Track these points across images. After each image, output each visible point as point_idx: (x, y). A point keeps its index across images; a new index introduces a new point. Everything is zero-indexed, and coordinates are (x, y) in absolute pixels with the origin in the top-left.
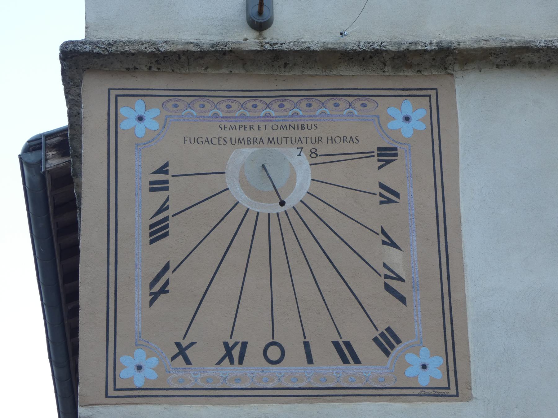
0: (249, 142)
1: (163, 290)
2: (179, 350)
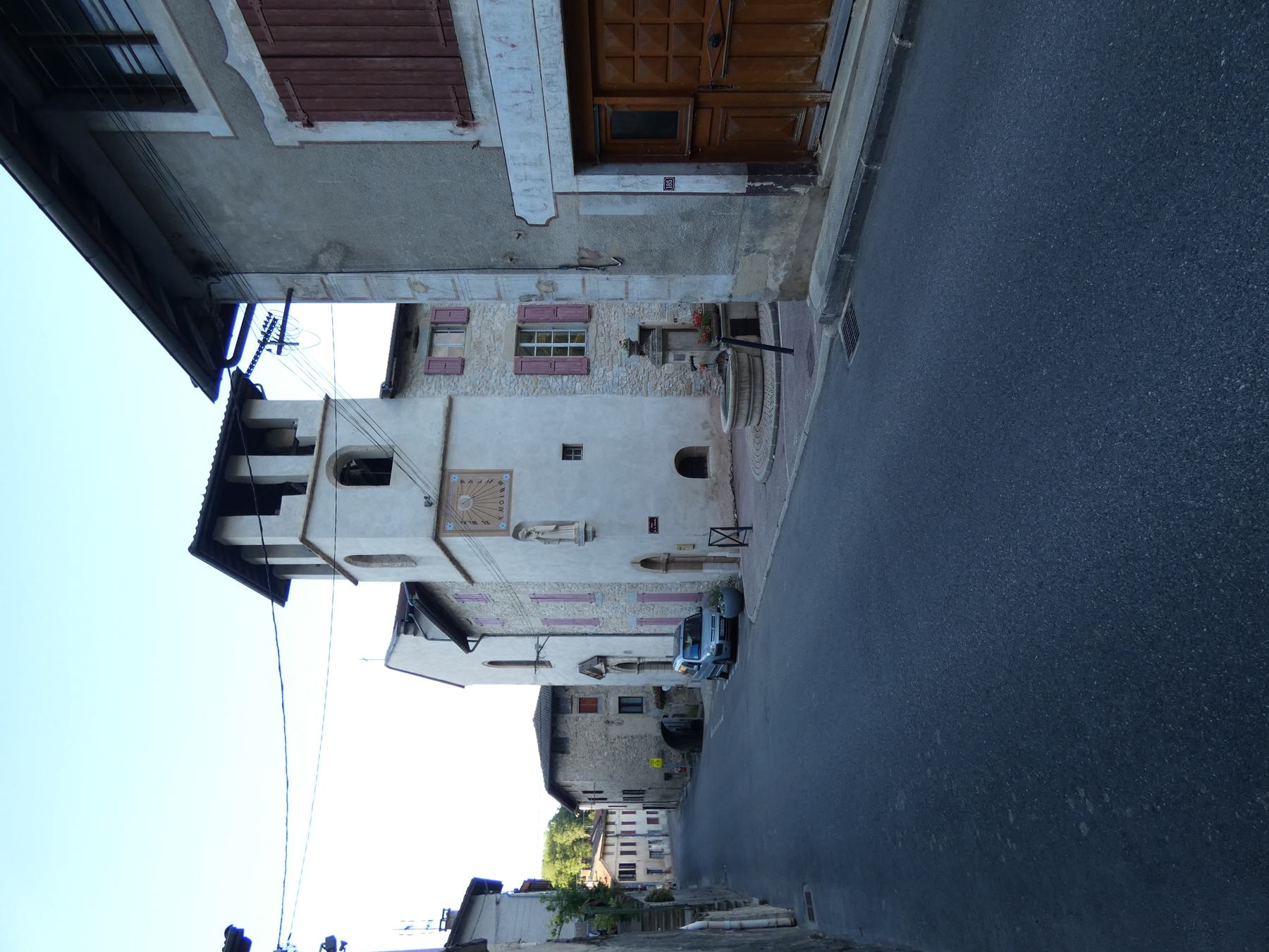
0: (457, 506)
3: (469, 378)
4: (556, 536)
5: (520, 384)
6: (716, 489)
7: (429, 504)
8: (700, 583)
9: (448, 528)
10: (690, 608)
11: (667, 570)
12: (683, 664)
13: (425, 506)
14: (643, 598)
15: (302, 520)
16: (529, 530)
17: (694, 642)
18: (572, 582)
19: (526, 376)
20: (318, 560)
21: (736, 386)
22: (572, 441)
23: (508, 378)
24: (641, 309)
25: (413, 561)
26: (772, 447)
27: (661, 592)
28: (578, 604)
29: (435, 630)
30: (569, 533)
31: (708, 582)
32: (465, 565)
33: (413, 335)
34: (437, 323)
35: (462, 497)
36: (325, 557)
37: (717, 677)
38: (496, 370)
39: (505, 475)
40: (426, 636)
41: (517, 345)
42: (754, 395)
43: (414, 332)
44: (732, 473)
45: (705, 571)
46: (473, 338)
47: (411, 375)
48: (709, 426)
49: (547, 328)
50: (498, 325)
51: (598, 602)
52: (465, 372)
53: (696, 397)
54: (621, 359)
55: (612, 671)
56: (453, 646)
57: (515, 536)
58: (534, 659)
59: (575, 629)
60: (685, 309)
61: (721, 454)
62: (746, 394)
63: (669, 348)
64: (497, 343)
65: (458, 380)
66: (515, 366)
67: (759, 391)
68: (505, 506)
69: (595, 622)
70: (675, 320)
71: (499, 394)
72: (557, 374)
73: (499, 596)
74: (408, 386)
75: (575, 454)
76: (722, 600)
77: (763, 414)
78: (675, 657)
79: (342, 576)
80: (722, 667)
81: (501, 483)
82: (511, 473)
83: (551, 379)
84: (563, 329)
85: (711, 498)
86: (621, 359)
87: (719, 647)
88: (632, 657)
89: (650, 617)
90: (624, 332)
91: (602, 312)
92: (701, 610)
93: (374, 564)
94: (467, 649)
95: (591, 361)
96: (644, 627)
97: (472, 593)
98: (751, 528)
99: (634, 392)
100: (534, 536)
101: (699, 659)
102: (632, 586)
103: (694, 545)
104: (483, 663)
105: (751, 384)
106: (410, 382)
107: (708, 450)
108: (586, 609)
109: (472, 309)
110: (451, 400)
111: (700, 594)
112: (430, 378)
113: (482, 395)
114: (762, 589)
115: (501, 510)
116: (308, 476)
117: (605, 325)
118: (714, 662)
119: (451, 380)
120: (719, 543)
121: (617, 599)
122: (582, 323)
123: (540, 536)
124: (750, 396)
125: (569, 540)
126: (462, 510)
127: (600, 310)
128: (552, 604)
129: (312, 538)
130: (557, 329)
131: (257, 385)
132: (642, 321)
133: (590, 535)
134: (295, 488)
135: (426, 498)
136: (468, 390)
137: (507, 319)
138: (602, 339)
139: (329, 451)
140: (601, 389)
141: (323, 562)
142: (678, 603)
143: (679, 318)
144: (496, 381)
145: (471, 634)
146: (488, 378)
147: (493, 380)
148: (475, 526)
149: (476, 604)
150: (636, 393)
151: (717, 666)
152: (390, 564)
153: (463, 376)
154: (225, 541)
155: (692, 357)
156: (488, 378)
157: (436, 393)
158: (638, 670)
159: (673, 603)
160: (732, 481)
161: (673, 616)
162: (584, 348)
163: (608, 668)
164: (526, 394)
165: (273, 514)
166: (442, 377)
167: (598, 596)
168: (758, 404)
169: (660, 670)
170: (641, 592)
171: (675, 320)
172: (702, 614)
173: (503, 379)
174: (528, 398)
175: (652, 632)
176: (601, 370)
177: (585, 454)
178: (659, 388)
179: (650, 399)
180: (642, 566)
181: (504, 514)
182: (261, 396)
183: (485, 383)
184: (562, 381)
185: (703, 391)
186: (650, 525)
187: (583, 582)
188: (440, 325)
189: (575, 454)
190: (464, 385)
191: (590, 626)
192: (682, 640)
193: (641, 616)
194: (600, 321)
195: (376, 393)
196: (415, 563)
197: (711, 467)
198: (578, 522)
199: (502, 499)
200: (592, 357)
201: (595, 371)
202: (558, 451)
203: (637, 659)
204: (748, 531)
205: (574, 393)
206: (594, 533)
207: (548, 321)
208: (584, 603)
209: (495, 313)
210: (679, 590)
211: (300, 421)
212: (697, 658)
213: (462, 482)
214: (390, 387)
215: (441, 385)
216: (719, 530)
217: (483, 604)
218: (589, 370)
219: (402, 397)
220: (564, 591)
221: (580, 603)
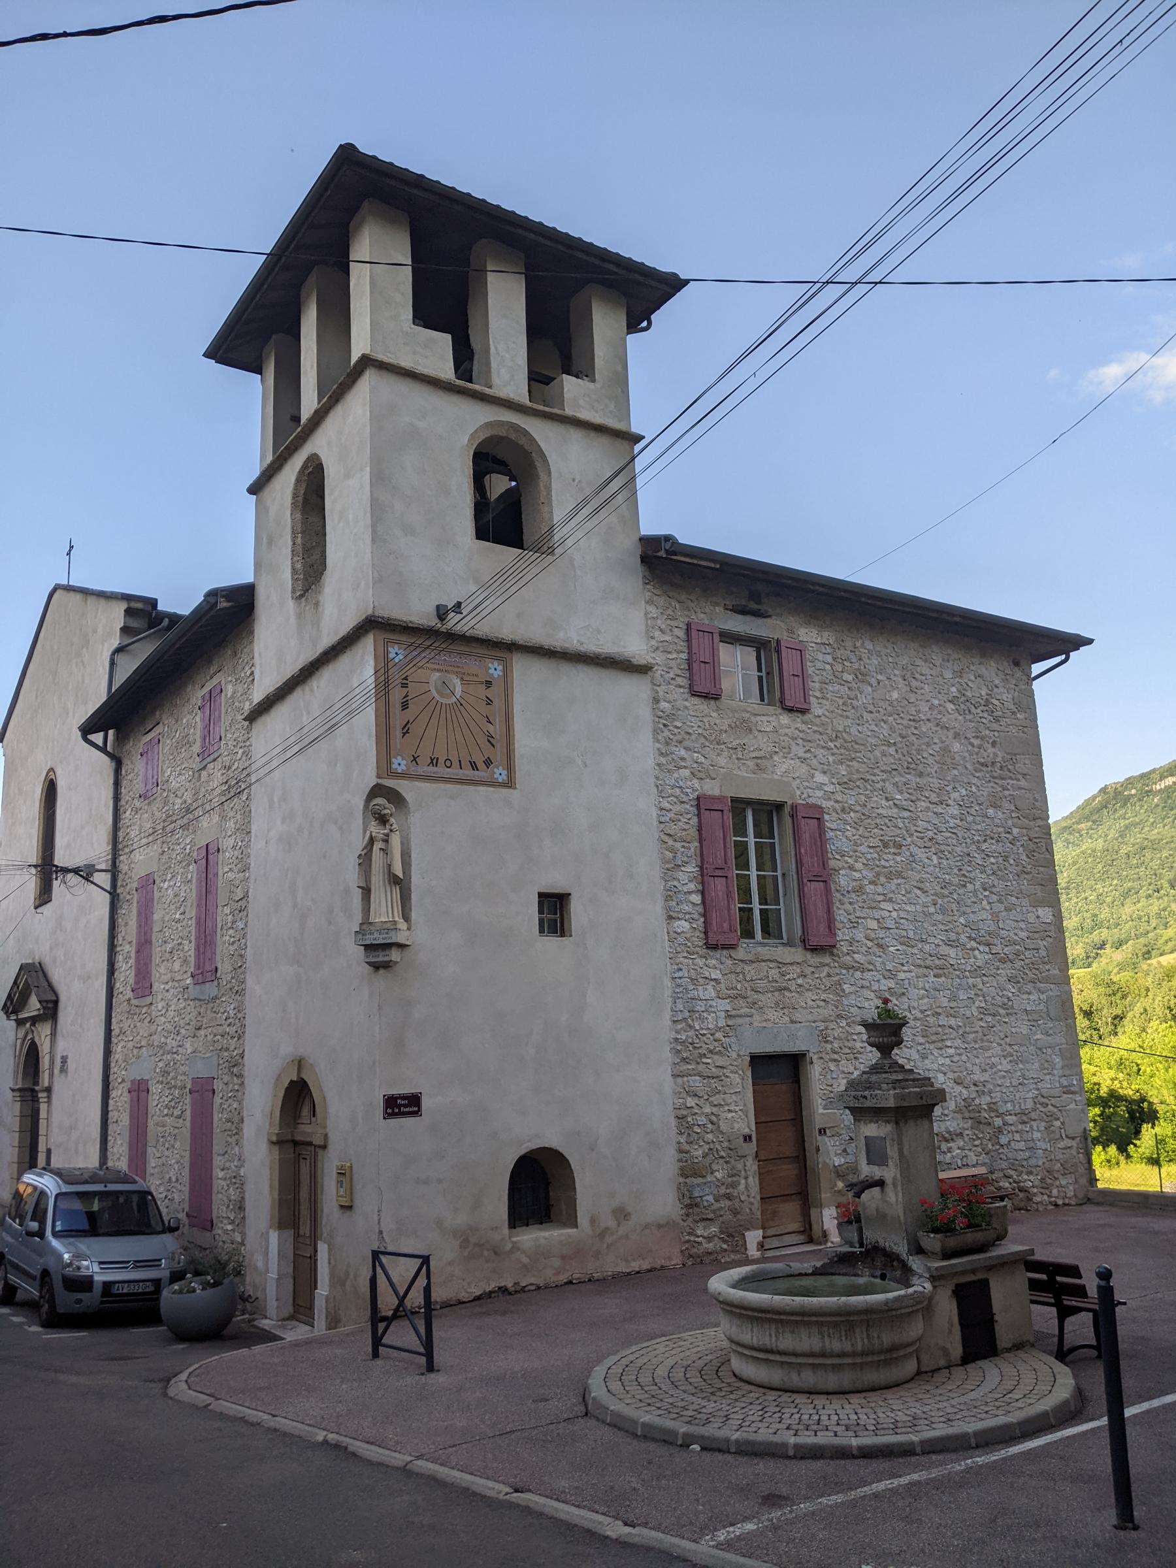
0: (439, 670)
1: (407, 732)
2: (1027, 705)
3: (686, 707)
4: (378, 881)
5: (678, 808)
6: (486, 1253)
7: (442, 613)
8: (240, 1224)
9: (393, 650)
10: (172, 1200)
11: (279, 1143)
12: (42, 1194)
13: (438, 607)
14: (203, 1091)
15: (406, 363)
16: (392, 820)
17: (91, 1216)
18: (248, 929)
19: (695, 820)
20: (309, 402)
21: (860, 1312)
22: (578, 911)
23: (689, 783)
24: (836, 1056)
25: (306, 591)
26: (727, 1440)
27: (216, 1131)
28: (189, 948)
29: (128, 667)
30: (384, 908)
31: (243, 1244)
32: (297, 697)
33: (753, 606)
34: (778, 651)
35: (457, 682)
36: (319, 417)
37: (6, 1278)
38: (702, 759)
39: (505, 772)
40: (119, 650)
41: (748, 802)
42: (836, 1368)
43: (759, 607)
44: (523, 1289)
45: (274, 1237)
46: (759, 718)
47: (683, 597)
48: (619, 1225)
49: (786, 862)
50: (783, 766)
51: (194, 991)
52: (696, 700)
53: (679, 1189)
54: (740, 1016)
55: (21, 1033)
56: (97, 696)
57: (377, 791)
58: (60, 859)
59: (127, 948)
60: (845, 1150)
61: (563, 1257)
62: (835, 1344)
63: (902, 1125)
64: (751, 764)
65: (680, 687)
66: (713, 798)
67: (846, 1379)
68: (441, 770)
69: (143, 985)
70: (822, 1131)
71: (659, 765)
72: (703, 883)
73: (216, 777)
74: (665, 592)
75: (549, 920)
76: (206, 1286)
77: (762, 1390)
78: (58, 1173)
79: (270, 458)
80: (31, 1290)
81: (488, 763)
82: (509, 784)
83: (692, 868)
84: (785, 895)
85: (465, 1243)
86: (740, 1016)
87: (86, 1284)
88: (51, 1075)
89: (151, 1111)
90: (792, 1022)
91: (824, 974)
92: (172, 1230)
93: (299, 516)
94: (87, 730)
95: (733, 953)
96: (126, 1097)
97: (225, 721)
98: (430, 1368)
99: (679, 1048)
100: (375, 829)
101: (55, 1234)
102: (235, 1066)
103: (350, 1208)
104: (52, 770)
105: (864, 1354)
106: (671, 594)
107: (565, 1225)
108: (177, 966)
109: (807, 717)
110: (643, 670)
111: (209, 1225)
112: (681, 633)
113: (656, 732)
114: (281, 1423)
115: (434, 762)
116: (490, 387)
117: (800, 981)
118: (45, 1273)
119: (679, 672)
120: (381, 1279)
121: (202, 1032)
122: (800, 933)
123: (378, 846)
124: (832, 1355)
125: (366, 910)
126: (432, 683)
127: (826, 969)
128: (190, 893)
129: (368, 381)
130: (784, 886)
131: (650, 323)
132: (815, 1058)
133: (381, 957)
134: (464, 356)
135: (459, 604)
136: (663, 705)
137: (795, 784)
138: (774, 973)
139: (543, 434)
140: (680, 974)
141: (306, 412)
142: (186, 1172)
143: (827, 1139)
144: (683, 759)
145: (121, 739)
146: (686, 743)
147: (683, 752)
148: (398, 706)
149: (196, 734)
150: (679, 1052)
151: (34, 1278)
152: (299, 549)
153: (686, 696)
154: (359, 226)
155: (881, 1183)
156: (686, 743)
157: (653, 642)
158: (20, 1090)
159: (186, 1161)
160: (503, 1290)
161: (152, 1162)
162: (754, 938)
163: (28, 1025)
164: (663, 819)
165: (415, 317)
166: (684, 656)
167: (211, 989)
168: (808, 1378)
169: (17, 1135)
170: (218, 1085)
171: (822, 1131)
172: (163, 1232)
173: (686, 773)
174: (655, 823)
175: (113, 1116)
176: (716, 974)
177: (552, 942)
178: (691, 1102)
179: (669, 1084)
180: (292, 1082)
181: (424, 769)
182: (633, 326)
183: (679, 737)
184: (690, 893)
185: (691, 1205)
186: (403, 1097)
187: (249, 953)
188: (775, 656)
189: (549, 920)
190: (670, 697)
191: (131, 980)
192: (99, 1187)
193: (155, 1088)
194: (808, 970)
195: (648, 527)
196: (301, 596)
197: (532, 1237)
198: (409, 929)
199: (456, 763)
200: (740, 953)
201: (714, 962)
202: (555, 882)
203: (46, 1084)
204: (423, 1360)
205: (670, 918)
206: (387, 965)
207: (799, 864)
208: (192, 960)
209: (803, 760)
210: (221, 1174)
211: (591, 385)
212: (58, 1228)
213: (489, 684)
214: (667, 551)
215: (669, 653)
216: (421, 1282)
217: (196, 748)
218: (715, 947)
219: (644, 577)
220: (224, 914)
221: (192, 953)
